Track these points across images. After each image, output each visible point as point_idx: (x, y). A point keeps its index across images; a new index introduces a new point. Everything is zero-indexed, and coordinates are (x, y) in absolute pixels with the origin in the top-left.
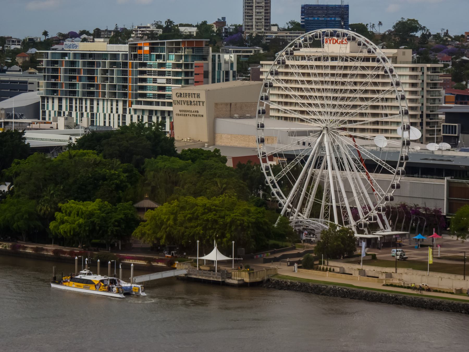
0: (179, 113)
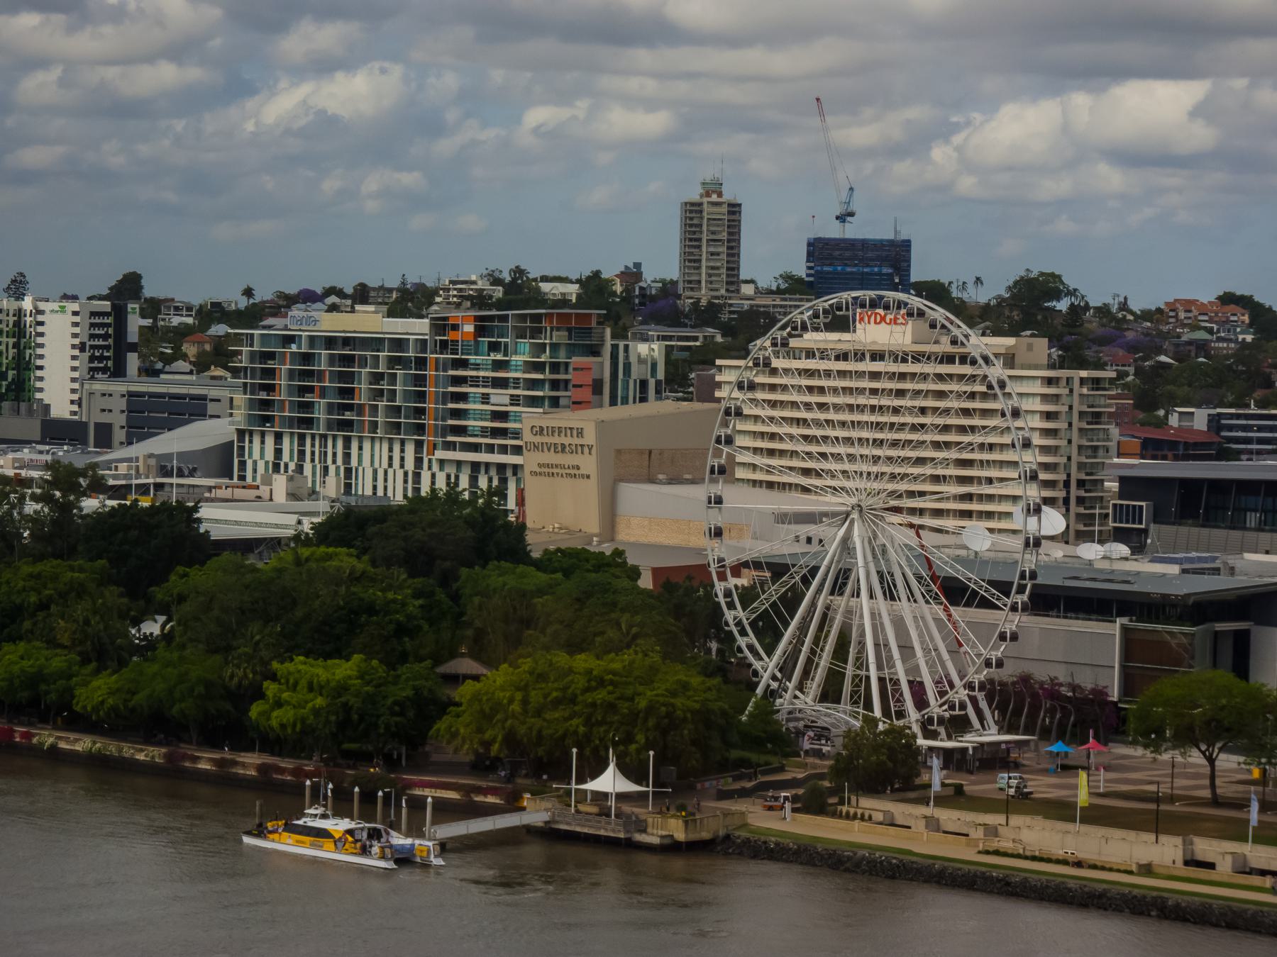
0: (538, 470)
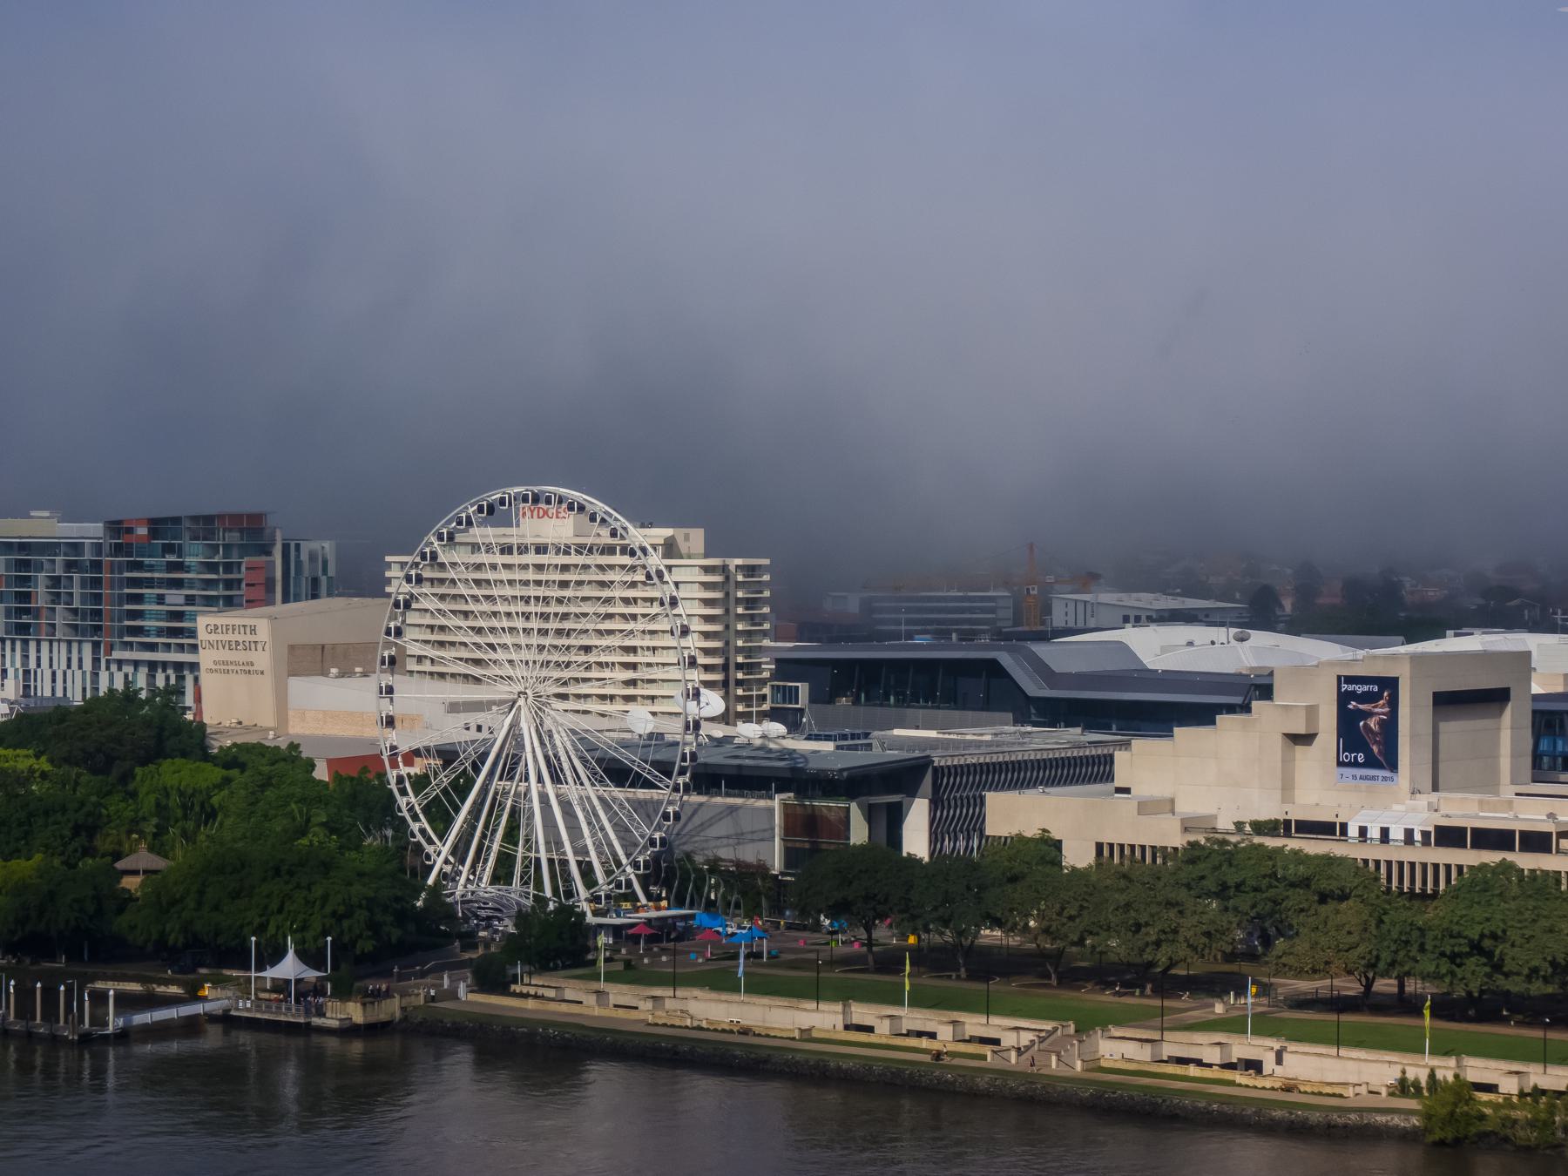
0: (214, 667)
